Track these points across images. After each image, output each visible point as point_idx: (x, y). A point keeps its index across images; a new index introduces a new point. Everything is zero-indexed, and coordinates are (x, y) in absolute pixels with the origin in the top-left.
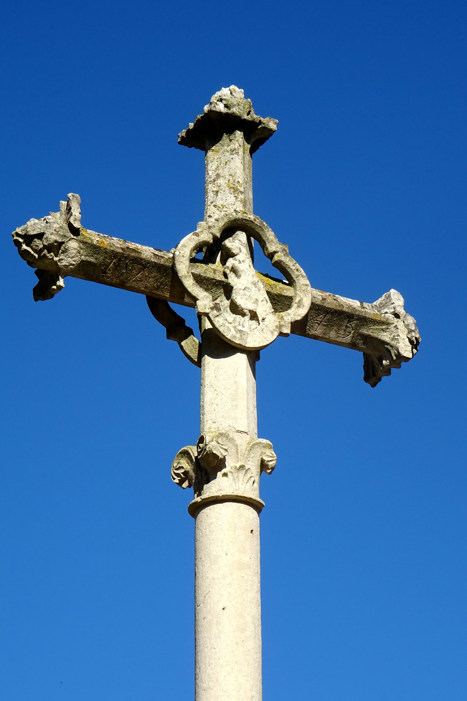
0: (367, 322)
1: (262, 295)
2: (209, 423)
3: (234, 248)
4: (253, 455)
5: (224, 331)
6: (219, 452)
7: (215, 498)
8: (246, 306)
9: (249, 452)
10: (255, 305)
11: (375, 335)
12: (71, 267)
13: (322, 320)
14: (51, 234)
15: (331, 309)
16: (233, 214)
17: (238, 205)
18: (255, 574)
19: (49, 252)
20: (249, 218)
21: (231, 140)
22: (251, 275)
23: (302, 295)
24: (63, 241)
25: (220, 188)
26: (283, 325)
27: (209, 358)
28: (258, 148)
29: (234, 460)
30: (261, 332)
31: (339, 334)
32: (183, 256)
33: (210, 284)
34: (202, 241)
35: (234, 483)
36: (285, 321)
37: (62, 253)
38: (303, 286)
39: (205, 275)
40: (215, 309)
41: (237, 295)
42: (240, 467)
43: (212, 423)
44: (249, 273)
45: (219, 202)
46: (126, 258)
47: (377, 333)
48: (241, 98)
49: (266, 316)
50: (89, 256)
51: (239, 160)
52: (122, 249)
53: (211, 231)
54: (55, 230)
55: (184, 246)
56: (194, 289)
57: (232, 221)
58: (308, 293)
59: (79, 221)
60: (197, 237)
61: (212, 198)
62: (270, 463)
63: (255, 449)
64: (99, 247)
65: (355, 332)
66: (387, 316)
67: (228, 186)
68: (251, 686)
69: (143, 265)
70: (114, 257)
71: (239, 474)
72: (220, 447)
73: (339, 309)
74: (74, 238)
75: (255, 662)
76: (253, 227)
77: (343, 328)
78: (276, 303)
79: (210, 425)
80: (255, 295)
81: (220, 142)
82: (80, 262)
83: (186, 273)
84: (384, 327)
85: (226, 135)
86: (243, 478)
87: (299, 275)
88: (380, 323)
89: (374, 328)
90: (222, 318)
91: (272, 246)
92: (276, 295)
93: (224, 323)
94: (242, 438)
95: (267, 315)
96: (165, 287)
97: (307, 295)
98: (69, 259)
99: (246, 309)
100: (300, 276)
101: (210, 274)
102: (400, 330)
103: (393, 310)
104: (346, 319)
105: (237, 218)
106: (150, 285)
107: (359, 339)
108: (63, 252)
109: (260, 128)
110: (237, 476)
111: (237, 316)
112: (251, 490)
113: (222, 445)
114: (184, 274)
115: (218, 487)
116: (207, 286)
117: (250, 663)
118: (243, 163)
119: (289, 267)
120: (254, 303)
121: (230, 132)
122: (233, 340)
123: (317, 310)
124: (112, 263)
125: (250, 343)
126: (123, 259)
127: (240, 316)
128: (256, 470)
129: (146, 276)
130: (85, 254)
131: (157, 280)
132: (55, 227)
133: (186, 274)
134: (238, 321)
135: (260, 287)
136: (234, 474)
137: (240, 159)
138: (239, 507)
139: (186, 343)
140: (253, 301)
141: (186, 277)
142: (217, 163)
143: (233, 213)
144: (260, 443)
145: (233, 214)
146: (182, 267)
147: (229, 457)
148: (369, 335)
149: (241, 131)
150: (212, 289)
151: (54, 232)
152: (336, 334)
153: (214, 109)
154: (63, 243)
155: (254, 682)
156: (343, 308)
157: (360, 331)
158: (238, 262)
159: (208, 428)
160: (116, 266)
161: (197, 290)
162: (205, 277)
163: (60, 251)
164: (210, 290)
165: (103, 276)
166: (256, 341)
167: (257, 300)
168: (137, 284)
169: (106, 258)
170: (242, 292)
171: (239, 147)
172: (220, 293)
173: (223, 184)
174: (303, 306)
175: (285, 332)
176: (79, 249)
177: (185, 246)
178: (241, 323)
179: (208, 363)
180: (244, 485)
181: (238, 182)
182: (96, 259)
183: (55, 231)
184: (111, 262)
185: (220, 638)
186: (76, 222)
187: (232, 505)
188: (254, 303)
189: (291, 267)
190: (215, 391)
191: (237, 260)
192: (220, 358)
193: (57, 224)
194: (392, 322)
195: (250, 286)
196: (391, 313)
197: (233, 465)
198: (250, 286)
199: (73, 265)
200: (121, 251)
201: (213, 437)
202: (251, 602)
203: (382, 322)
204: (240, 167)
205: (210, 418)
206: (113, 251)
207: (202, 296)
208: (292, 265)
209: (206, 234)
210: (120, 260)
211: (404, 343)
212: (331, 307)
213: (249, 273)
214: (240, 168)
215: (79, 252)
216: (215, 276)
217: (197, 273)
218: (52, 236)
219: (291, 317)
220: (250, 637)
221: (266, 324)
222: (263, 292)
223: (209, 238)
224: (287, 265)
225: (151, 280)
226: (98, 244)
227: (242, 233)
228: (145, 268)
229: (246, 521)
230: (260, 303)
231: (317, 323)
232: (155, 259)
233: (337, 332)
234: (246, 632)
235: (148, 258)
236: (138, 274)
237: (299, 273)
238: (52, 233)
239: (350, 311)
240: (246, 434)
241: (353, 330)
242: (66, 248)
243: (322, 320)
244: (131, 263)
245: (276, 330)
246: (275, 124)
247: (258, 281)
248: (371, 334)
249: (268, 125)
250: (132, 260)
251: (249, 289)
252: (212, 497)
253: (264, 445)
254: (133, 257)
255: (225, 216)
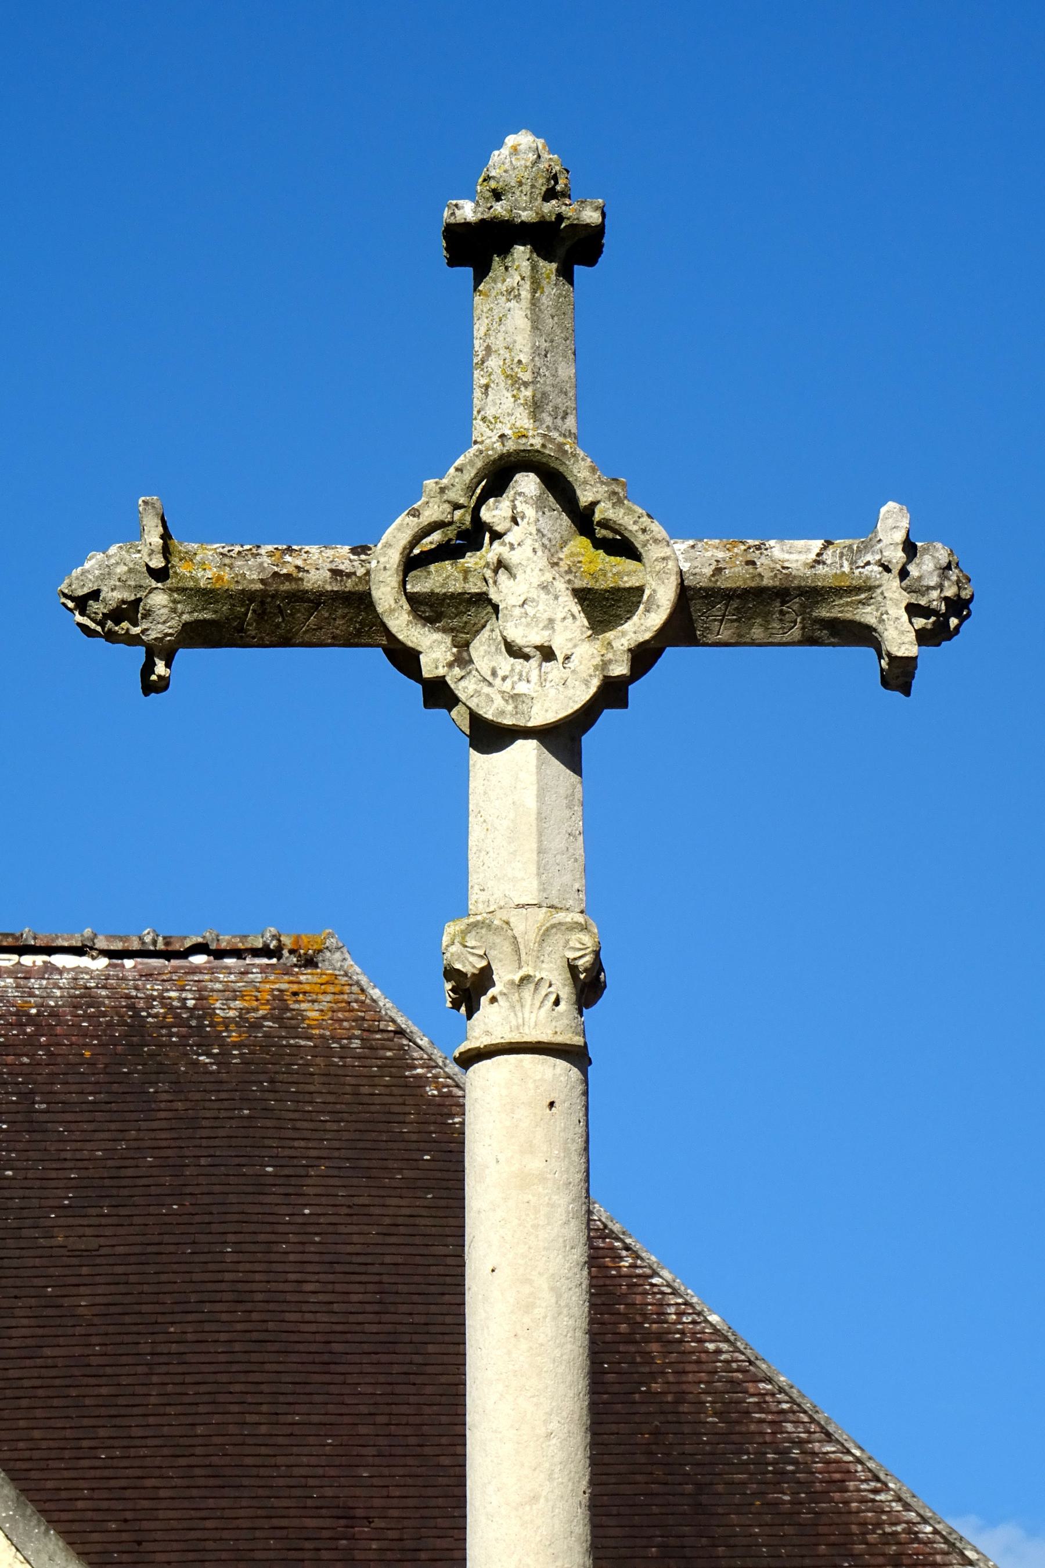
0: (822, 595)
1: (564, 608)
2: (474, 892)
3: (498, 522)
4: (551, 949)
5: (478, 705)
6: (467, 964)
7: (474, 1053)
8: (527, 639)
9: (540, 945)
10: (546, 633)
11: (849, 616)
12: (169, 638)
13: (725, 613)
14: (112, 590)
15: (735, 590)
16: (495, 446)
17: (519, 416)
18: (558, 1189)
19: (117, 623)
20: (532, 445)
21: (507, 268)
22: (537, 571)
23: (654, 583)
24: (138, 596)
25: (492, 377)
26: (610, 661)
27: (475, 752)
28: (602, 246)
29: (510, 968)
30: (561, 688)
31: (772, 628)
32: (385, 568)
33: (460, 604)
34: (426, 523)
35: (512, 1014)
36: (615, 651)
37: (142, 618)
38: (656, 563)
39: (444, 591)
40: (456, 664)
41: (507, 621)
42: (522, 980)
43: (479, 892)
44: (533, 566)
45: (489, 409)
46: (273, 597)
47: (852, 611)
48: (526, 167)
49: (573, 651)
50: (200, 611)
51: (521, 312)
52: (262, 581)
53: (445, 498)
54: (119, 580)
55: (388, 545)
56: (409, 632)
57: (494, 461)
58: (668, 576)
59: (159, 553)
60: (416, 519)
61: (478, 402)
62: (580, 962)
63: (551, 938)
64: (212, 591)
65: (803, 619)
66: (866, 573)
67: (504, 372)
68: (546, 1413)
69: (312, 601)
70: (249, 600)
71: (522, 994)
72: (470, 953)
73: (753, 584)
74: (157, 588)
75: (556, 1364)
76: (544, 460)
77: (774, 616)
78: (614, 605)
79: (477, 896)
80: (545, 611)
81: (490, 274)
82: (182, 627)
83: (392, 602)
84: (863, 596)
85: (497, 259)
86: (533, 998)
87: (648, 540)
88: (851, 590)
89: (842, 602)
90: (473, 680)
91: (586, 493)
92: (606, 591)
93: (478, 689)
94: (527, 919)
95: (575, 646)
96: (371, 628)
97: (666, 581)
98: (160, 626)
99: (528, 646)
100: (651, 542)
101: (455, 585)
102: (891, 599)
103: (878, 557)
104: (774, 600)
105: (505, 451)
106: (342, 631)
107: (819, 630)
108: (145, 616)
109: (565, 227)
110: (518, 998)
111: (517, 660)
112: (549, 1019)
113: (472, 948)
114: (387, 607)
115: (482, 1026)
116: (457, 608)
117: (545, 1369)
118: (529, 316)
119: (626, 529)
120: (545, 628)
121: (505, 251)
122: (499, 720)
123: (705, 597)
124: (250, 612)
125: (536, 716)
126: (269, 600)
127: (521, 661)
128: (560, 977)
129: (326, 618)
130: (188, 609)
131: (351, 619)
132: (120, 574)
133: (393, 606)
134: (517, 671)
135: (557, 590)
136: (510, 996)
137: (524, 308)
138: (521, 1061)
139: (459, 712)
140: (541, 625)
141: (392, 611)
142: (486, 321)
143: (495, 443)
144: (560, 923)
145: (495, 446)
146: (383, 594)
147: (499, 964)
148: (836, 619)
149: (524, 245)
150: (469, 611)
151: (118, 583)
152: (764, 632)
153: (452, 220)
154: (139, 600)
155: (554, 1404)
156: (762, 580)
157: (814, 614)
158: (507, 548)
159: (473, 902)
160: (259, 614)
161: (416, 634)
162: (445, 594)
163: (139, 615)
164: (465, 613)
165: (242, 637)
166: (550, 711)
167: (551, 621)
168: (314, 635)
169: (234, 606)
170: (517, 611)
171: (522, 282)
172: (487, 614)
173: (496, 369)
174: (658, 606)
175: (616, 675)
176: (171, 605)
177: (390, 545)
178: (524, 674)
179: (474, 765)
180: (535, 1011)
181: (520, 362)
182: (215, 612)
183: (119, 581)
184: (248, 610)
185: (488, 1328)
186: (153, 556)
187: (507, 1061)
188: (545, 628)
189: (630, 528)
190: (485, 824)
191: (505, 545)
192: (491, 753)
193: (125, 564)
194: (877, 583)
195: (534, 594)
196: (876, 564)
197: (510, 977)
198: (534, 594)
199: (171, 635)
200: (259, 586)
201: (454, 935)
202: (546, 1249)
203: (855, 587)
204: (522, 326)
205: (476, 881)
206: (243, 590)
207: (428, 644)
208: (631, 522)
209: (436, 507)
210: (262, 603)
211: (896, 628)
212: (734, 586)
213: (533, 567)
214: (523, 329)
215: (174, 610)
216: (467, 585)
217: (425, 590)
218: (115, 594)
219: (628, 638)
220: (545, 1317)
221: (573, 668)
222: (566, 599)
223: (443, 513)
224: (620, 525)
225: (339, 622)
226: (209, 586)
227: (527, 476)
228: (319, 604)
229: (537, 1087)
230: (558, 626)
231: (715, 620)
232: (334, 584)
233: (766, 628)
234: (536, 1311)
235: (319, 586)
236: (309, 619)
237: (648, 537)
238: (115, 586)
239: (778, 583)
240: (536, 909)
241: (797, 615)
242: (147, 608)
243: (725, 613)
244: (288, 604)
245: (595, 676)
246: (596, 210)
247: (554, 578)
248: (839, 615)
249: (578, 219)
250: (287, 597)
251: (533, 601)
252: (469, 1050)
253: (569, 925)
254: (285, 592)
255: (477, 456)
